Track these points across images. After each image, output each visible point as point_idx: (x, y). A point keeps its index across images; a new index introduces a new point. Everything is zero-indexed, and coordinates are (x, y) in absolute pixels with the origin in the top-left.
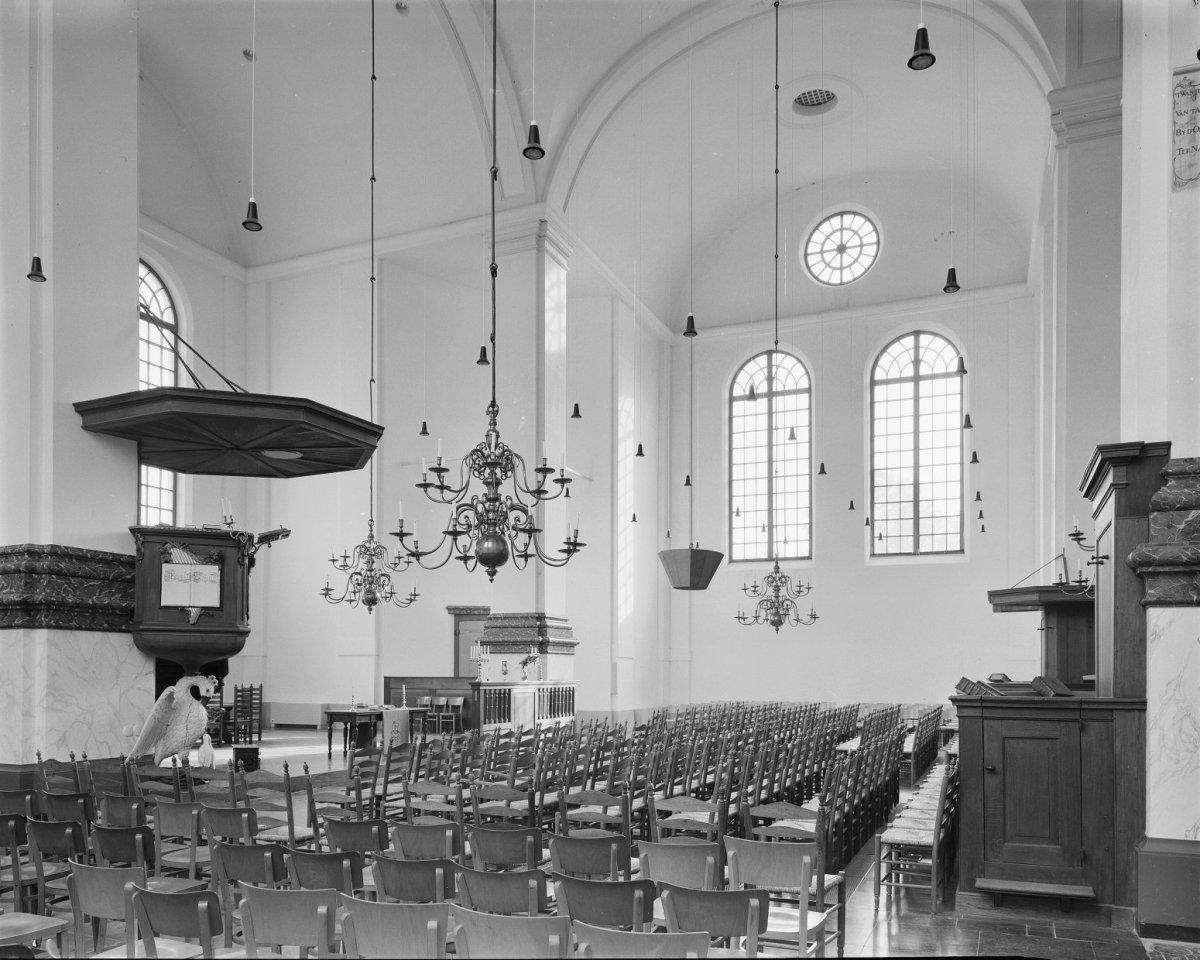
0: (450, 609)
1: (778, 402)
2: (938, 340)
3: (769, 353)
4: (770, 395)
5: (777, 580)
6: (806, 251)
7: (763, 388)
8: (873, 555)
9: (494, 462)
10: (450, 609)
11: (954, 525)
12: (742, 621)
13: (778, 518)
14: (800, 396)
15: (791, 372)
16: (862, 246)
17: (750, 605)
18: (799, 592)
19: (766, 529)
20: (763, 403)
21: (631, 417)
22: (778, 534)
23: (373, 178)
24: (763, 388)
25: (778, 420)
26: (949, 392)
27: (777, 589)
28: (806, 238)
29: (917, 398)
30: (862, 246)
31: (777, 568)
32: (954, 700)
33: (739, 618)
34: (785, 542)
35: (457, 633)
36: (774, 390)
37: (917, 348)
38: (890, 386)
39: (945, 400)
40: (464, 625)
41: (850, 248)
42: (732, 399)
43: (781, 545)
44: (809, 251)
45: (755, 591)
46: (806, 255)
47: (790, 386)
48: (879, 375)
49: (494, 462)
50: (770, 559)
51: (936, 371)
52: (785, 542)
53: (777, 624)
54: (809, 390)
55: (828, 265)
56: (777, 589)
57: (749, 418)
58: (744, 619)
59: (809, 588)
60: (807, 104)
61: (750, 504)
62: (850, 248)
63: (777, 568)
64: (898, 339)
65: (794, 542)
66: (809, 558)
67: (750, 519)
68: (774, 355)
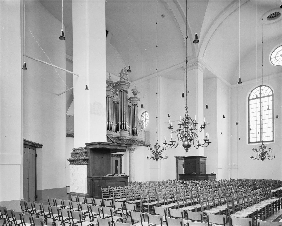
0: (176, 157)
1: (263, 99)
2: (266, 87)
3: (260, 86)
4: (261, 98)
5: (263, 148)
6: (271, 57)
7: (259, 96)
8: (249, 143)
9: (187, 121)
10: (176, 157)
11: (271, 134)
12: (252, 158)
13: (263, 130)
14: (270, 97)
15: (266, 91)
16: (276, 57)
17: (255, 155)
18: (163, 150)
19: (259, 133)
20: (259, 99)
21: (222, 107)
22: (263, 135)
23: (157, 23)
24: (259, 96)
25: (263, 104)
26: (257, 103)
27: (263, 150)
28: (271, 54)
29: (261, 103)
30: (276, 57)
31: (263, 144)
32: (69, 160)
33: (251, 158)
34: (265, 137)
35: (177, 163)
36: (262, 96)
37: (260, 90)
38: (266, 98)
39: (268, 102)
40: (179, 161)
41: (279, 56)
42: (249, 100)
43: (264, 138)
44: (271, 58)
45: (151, 150)
46: (271, 59)
47: (267, 95)
48: (251, 98)
49: (187, 121)
50: (261, 142)
51: (266, 95)
52: (265, 137)
53: (263, 159)
54: (273, 95)
55: (278, 60)
56: (263, 150)
57: (254, 105)
58: (253, 158)
59: (166, 149)
60: (273, 17)
61: (255, 127)
62: (279, 56)
63: (263, 144)
64: (256, 88)
65: (268, 136)
66: (273, 141)
67: (255, 131)
68: (262, 87)
